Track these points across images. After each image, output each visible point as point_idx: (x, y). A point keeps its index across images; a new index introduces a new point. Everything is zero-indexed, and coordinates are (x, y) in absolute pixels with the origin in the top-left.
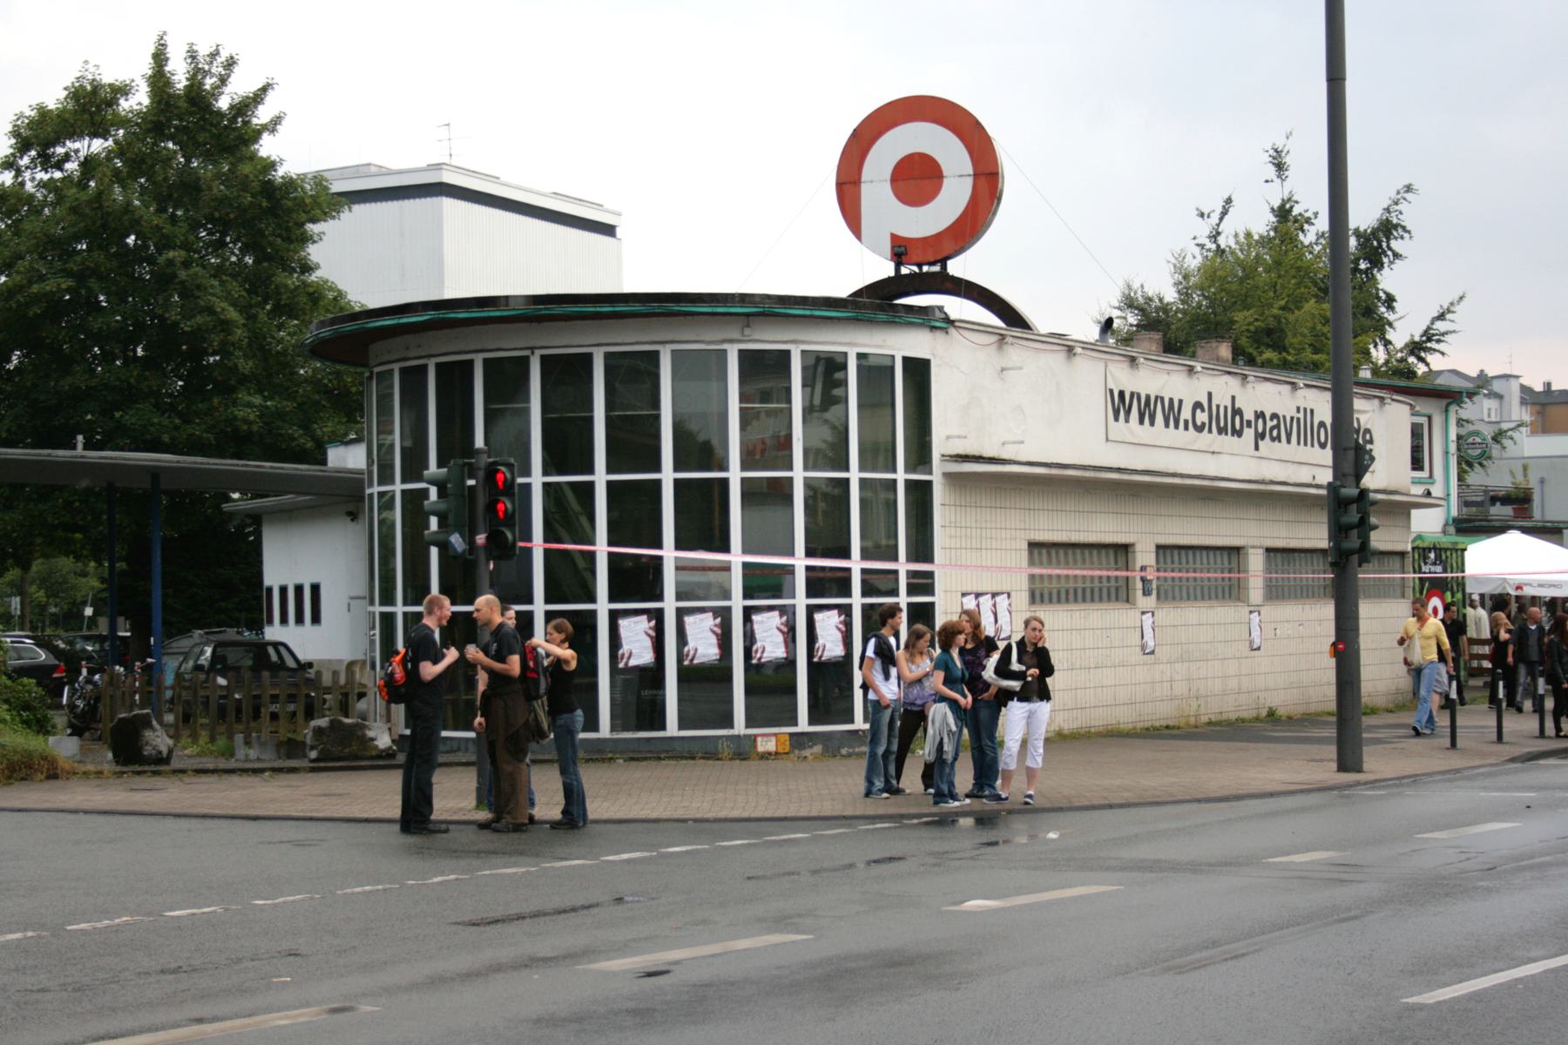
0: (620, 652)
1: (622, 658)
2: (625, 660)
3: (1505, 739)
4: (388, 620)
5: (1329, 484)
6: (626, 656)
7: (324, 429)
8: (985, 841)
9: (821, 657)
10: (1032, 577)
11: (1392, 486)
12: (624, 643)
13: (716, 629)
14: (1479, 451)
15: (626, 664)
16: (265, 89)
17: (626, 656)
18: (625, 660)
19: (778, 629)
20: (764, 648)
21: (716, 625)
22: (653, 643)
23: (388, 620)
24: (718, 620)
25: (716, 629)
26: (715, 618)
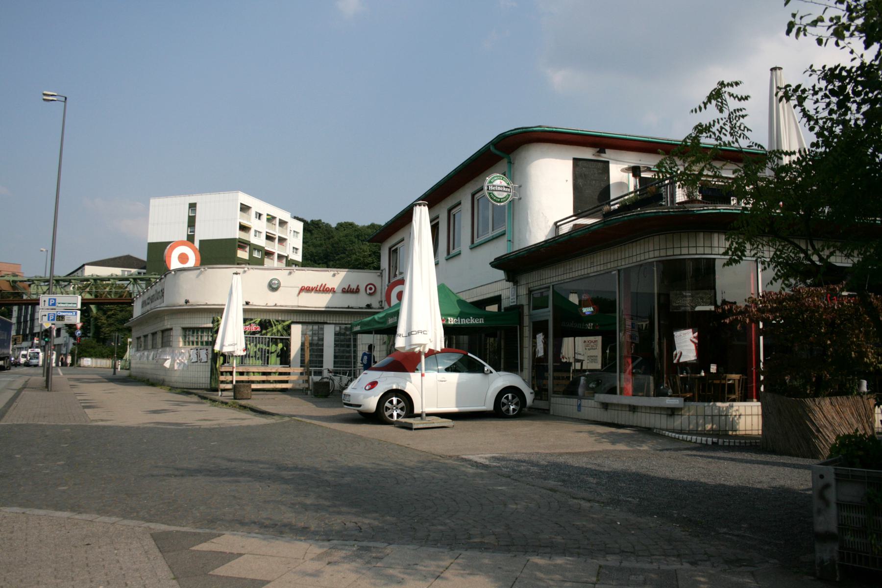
0: (675, 353)
1: (676, 357)
2: (677, 358)
3: (547, 408)
4: (354, 367)
5: (827, 82)
6: (678, 355)
7: (673, 169)
8: (686, 447)
9: (679, 360)
10: (322, 367)
11: (509, 252)
12: (677, 348)
13: (694, 340)
14: (505, 194)
15: (679, 360)
16: (299, 293)
17: (678, 355)
18: (677, 358)
19: (691, 340)
20: (681, 353)
21: (694, 337)
22: (696, 347)
23: (354, 367)
24: (696, 334)
25: (694, 340)
26: (694, 333)
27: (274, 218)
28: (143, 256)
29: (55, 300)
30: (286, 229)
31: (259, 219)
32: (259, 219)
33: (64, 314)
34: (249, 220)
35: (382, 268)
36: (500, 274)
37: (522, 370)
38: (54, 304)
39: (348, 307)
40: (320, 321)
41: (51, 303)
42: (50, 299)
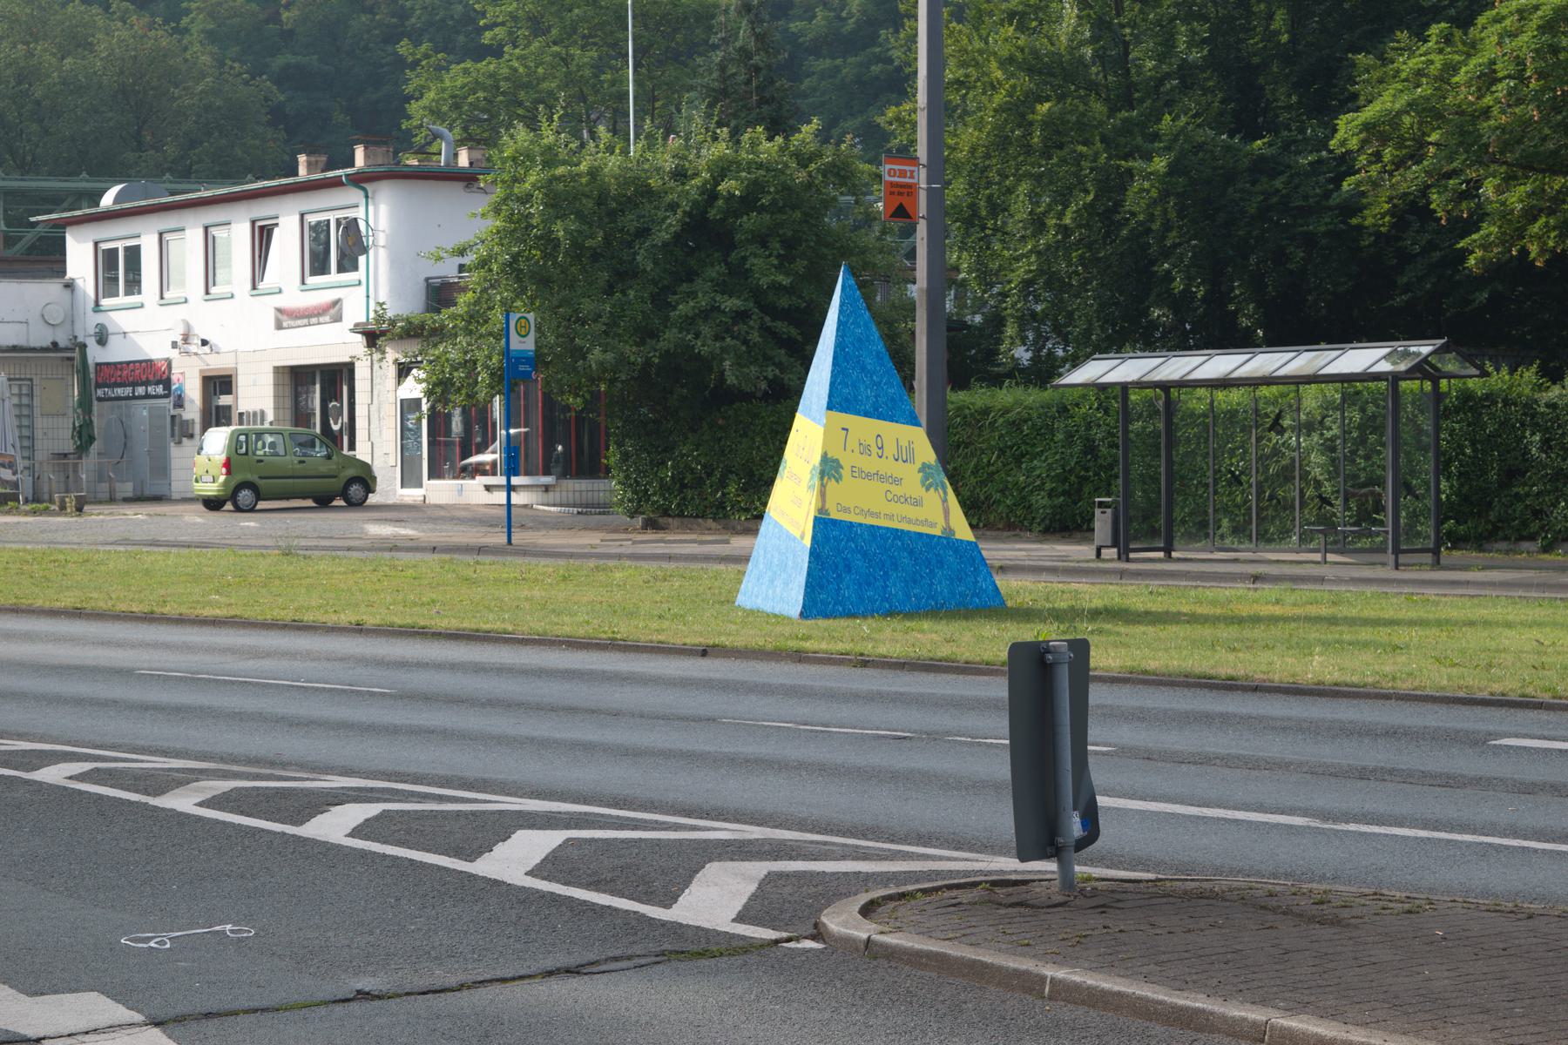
36: (360, 338)
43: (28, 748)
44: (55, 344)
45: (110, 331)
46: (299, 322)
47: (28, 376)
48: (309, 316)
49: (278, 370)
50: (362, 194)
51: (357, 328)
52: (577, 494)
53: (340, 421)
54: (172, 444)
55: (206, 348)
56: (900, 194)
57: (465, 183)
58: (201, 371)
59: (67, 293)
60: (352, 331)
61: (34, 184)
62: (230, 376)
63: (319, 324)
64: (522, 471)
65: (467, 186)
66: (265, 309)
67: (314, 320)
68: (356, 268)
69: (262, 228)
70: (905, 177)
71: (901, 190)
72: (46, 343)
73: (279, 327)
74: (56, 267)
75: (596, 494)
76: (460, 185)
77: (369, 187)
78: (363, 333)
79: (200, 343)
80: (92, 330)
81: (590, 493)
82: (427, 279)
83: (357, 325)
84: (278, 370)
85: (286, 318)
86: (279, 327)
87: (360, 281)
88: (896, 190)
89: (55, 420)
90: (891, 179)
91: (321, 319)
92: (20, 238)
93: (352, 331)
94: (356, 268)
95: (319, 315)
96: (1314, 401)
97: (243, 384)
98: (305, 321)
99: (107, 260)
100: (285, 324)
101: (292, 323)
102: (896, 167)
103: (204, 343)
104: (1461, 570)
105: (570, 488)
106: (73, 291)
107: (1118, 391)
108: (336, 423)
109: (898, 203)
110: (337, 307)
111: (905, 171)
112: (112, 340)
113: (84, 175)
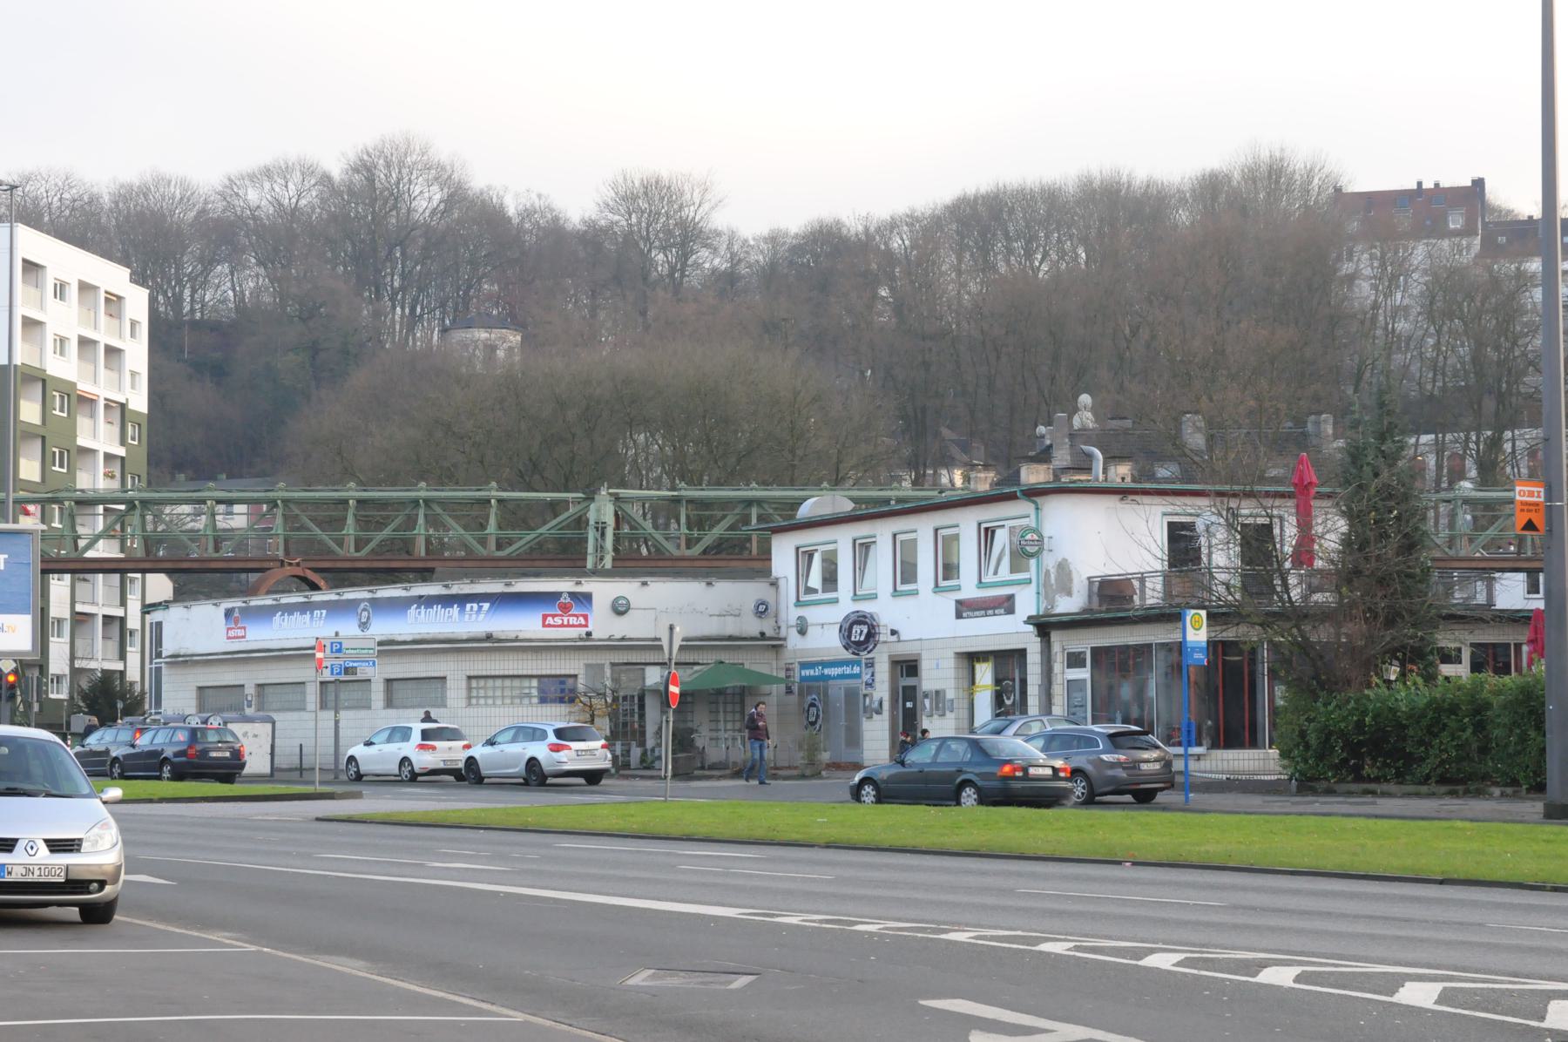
27: (94, 343)
28: (759, 636)
29: (340, 644)
30: (120, 371)
31: (62, 354)
32: (62, 354)
33: (355, 665)
34: (42, 307)
35: (774, 574)
37: (151, 624)
38: (339, 651)
39: (623, 639)
40: (630, 661)
41: (334, 648)
42: (332, 643)
43: (949, 1001)
44: (763, 634)
45: (810, 621)
46: (977, 613)
47: (740, 661)
48: (986, 609)
49: (919, 655)
50: (1033, 506)
51: (1030, 620)
52: (1225, 763)
53: (1012, 698)
54: (864, 719)
55: (894, 638)
56: (1529, 511)
57: (1121, 496)
58: (890, 656)
59: (772, 590)
60: (1025, 622)
61: (395, 494)
62: (916, 661)
63: (995, 615)
64: (1247, 744)
65: (1122, 499)
66: (948, 604)
67: (990, 612)
68: (1027, 570)
69: (987, 529)
70: (1533, 496)
71: (1531, 508)
72: (755, 632)
73: (959, 616)
74: (579, 563)
75: (1241, 762)
76: (1118, 497)
77: (1039, 500)
78: (1034, 625)
79: (889, 632)
80: (793, 621)
81: (1252, 762)
82: (1089, 578)
83: (1029, 618)
84: (919, 655)
85: (964, 609)
86: (959, 616)
87: (1030, 579)
88: (1526, 508)
89: (506, 709)
90: (1522, 499)
91: (996, 611)
92: (372, 540)
93: (1025, 622)
94: (1027, 570)
95: (994, 608)
96: (435, 188)
97: (926, 667)
98: (983, 612)
99: (805, 557)
100: (965, 615)
101: (970, 614)
102: (1526, 489)
103: (894, 632)
104: (552, 889)
105: (539, 713)
106: (777, 588)
107: (18, 719)
108: (1008, 699)
109: (1527, 519)
110: (1010, 602)
111: (1533, 492)
112: (810, 630)
113: (754, 485)
